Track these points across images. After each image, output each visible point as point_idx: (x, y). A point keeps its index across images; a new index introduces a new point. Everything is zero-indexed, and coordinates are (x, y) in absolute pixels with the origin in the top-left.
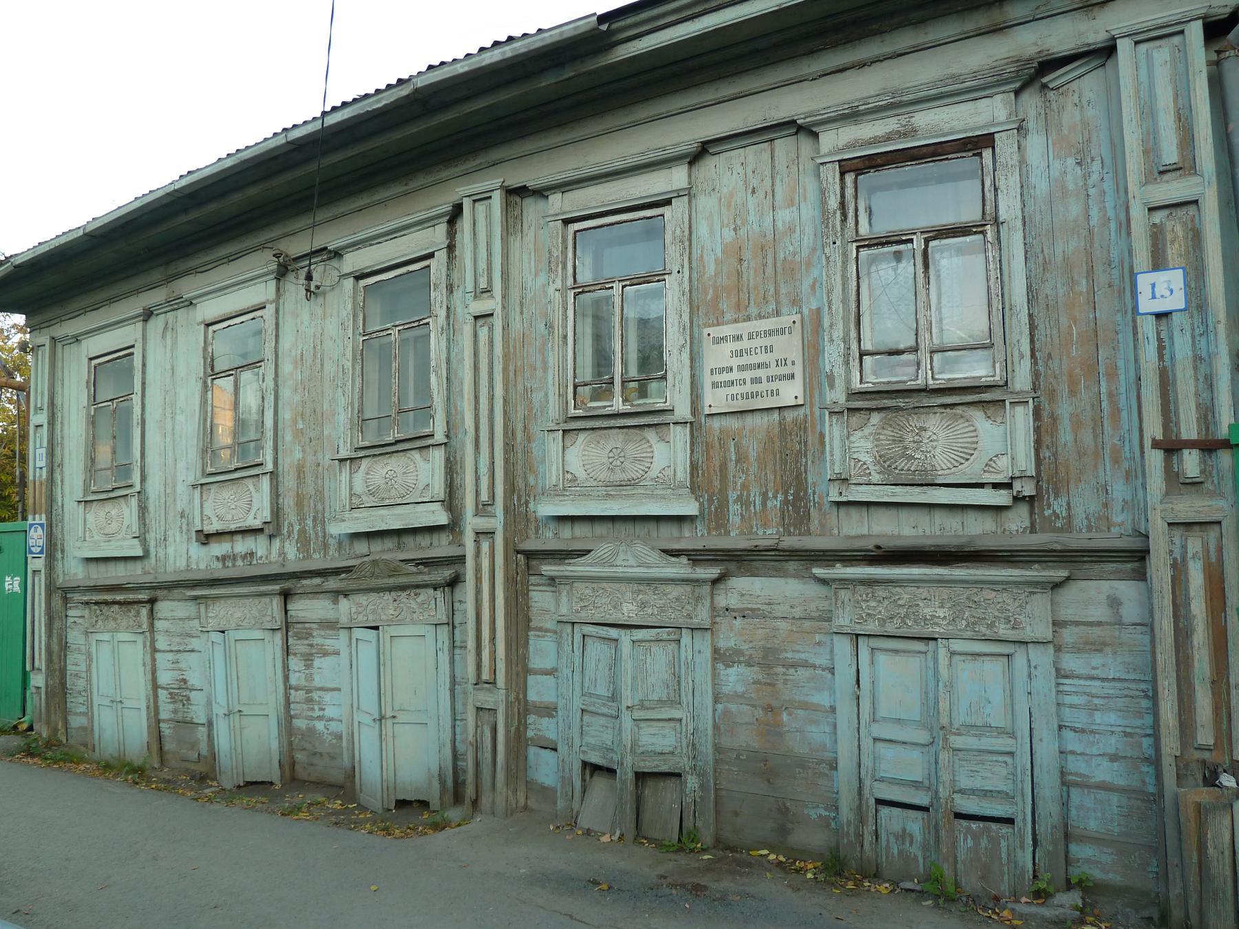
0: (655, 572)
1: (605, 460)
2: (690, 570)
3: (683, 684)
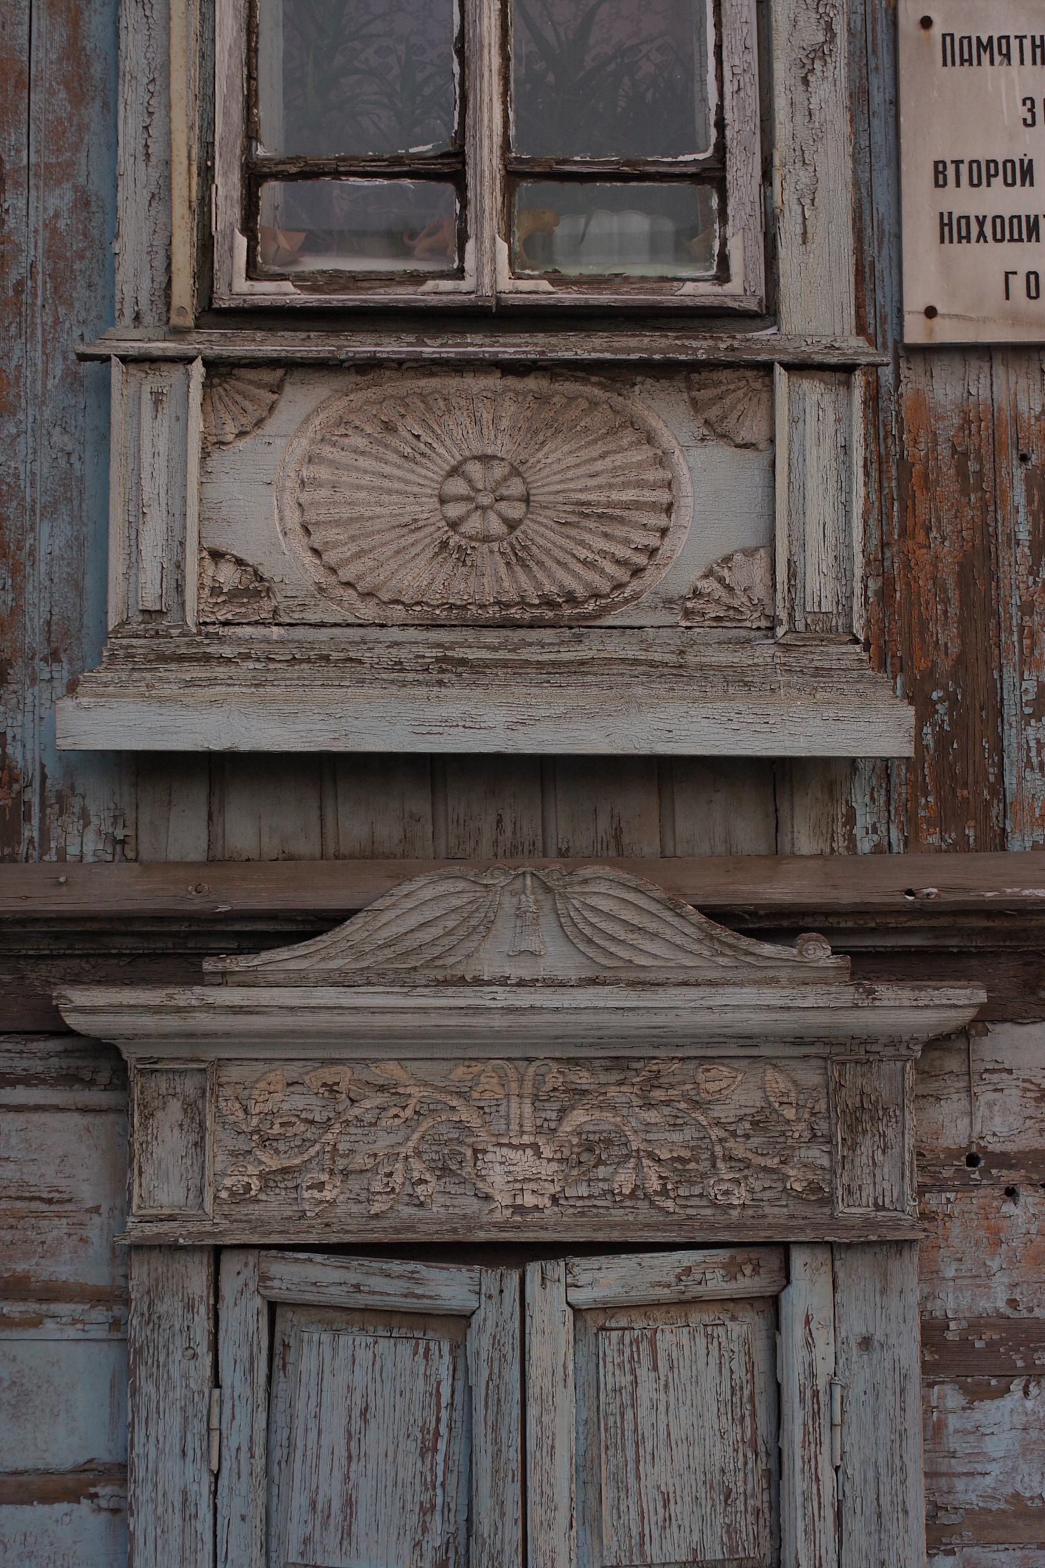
0: (681, 1009)
1: (426, 508)
2: (849, 995)
3: (797, 1482)
